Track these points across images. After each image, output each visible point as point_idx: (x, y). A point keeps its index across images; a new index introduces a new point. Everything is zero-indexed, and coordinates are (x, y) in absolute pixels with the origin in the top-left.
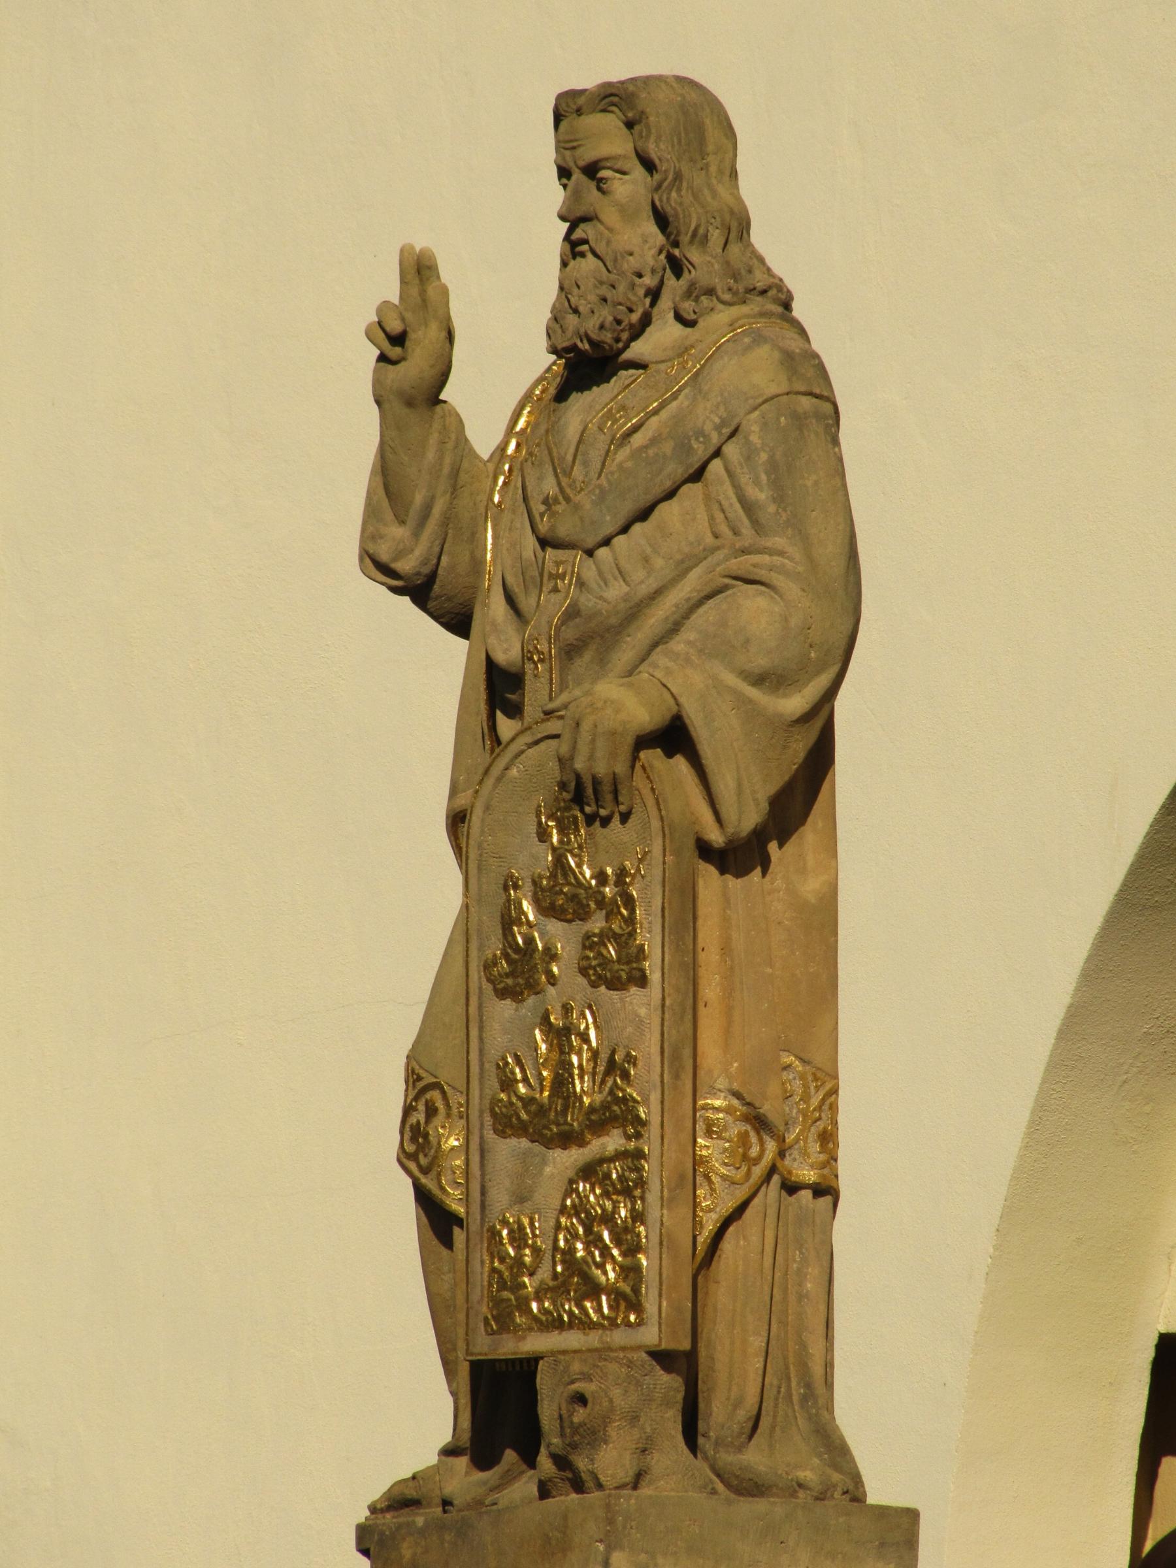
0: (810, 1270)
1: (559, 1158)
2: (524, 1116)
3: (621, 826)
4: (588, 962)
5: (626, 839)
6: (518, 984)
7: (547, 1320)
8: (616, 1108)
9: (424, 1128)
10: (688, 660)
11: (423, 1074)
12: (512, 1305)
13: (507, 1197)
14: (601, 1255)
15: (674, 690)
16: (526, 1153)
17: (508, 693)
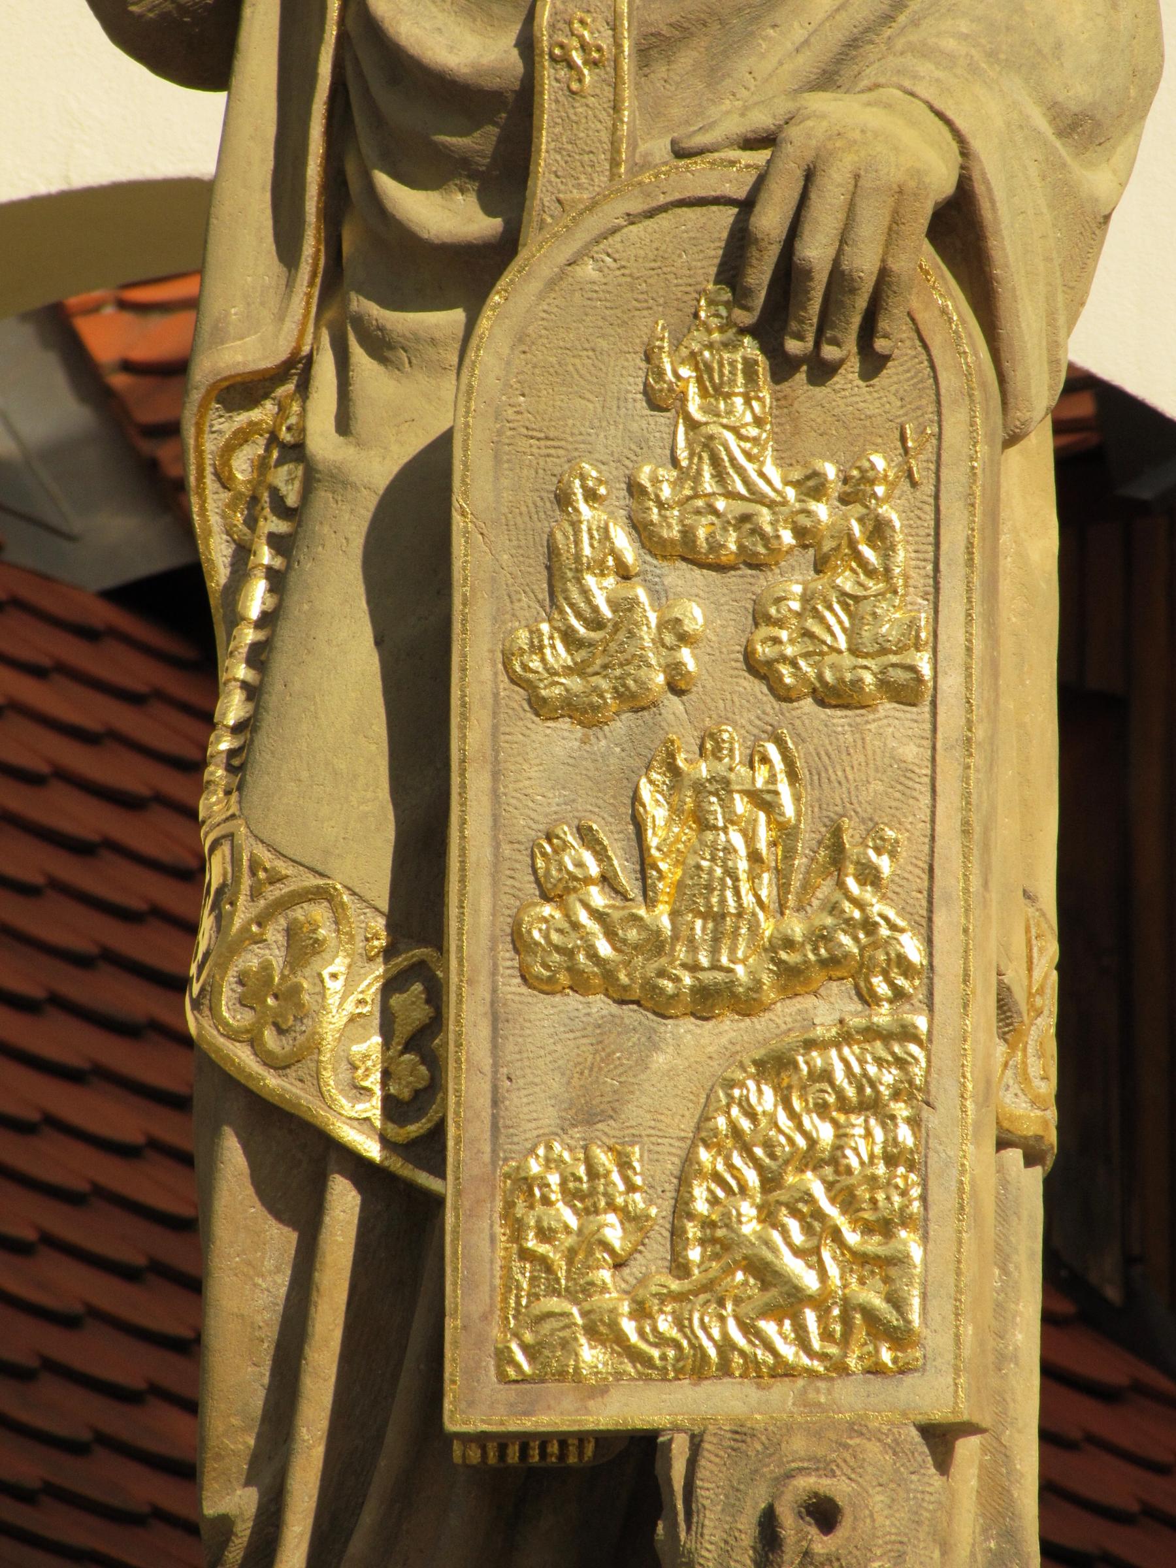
0: (1020, 1307)
1: (689, 1036)
2: (604, 949)
3: (861, 383)
4: (777, 647)
5: (872, 409)
6: (596, 690)
7: (663, 1357)
8: (845, 940)
9: (283, 978)
10: (973, 69)
11: (283, 867)
12: (575, 1324)
13: (552, 1112)
14: (808, 1230)
15: (960, 123)
16: (601, 1029)
17: (435, 134)
